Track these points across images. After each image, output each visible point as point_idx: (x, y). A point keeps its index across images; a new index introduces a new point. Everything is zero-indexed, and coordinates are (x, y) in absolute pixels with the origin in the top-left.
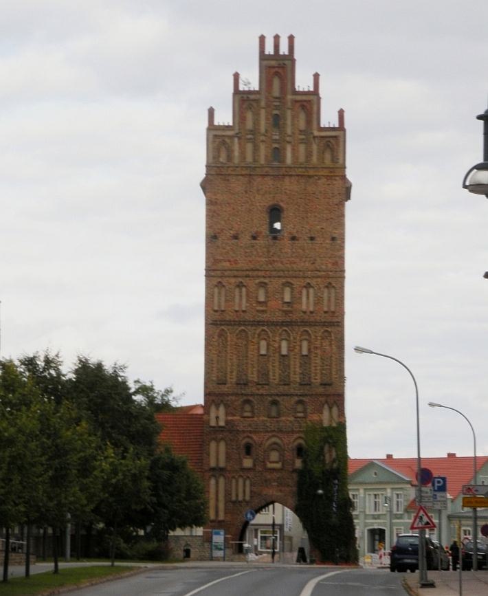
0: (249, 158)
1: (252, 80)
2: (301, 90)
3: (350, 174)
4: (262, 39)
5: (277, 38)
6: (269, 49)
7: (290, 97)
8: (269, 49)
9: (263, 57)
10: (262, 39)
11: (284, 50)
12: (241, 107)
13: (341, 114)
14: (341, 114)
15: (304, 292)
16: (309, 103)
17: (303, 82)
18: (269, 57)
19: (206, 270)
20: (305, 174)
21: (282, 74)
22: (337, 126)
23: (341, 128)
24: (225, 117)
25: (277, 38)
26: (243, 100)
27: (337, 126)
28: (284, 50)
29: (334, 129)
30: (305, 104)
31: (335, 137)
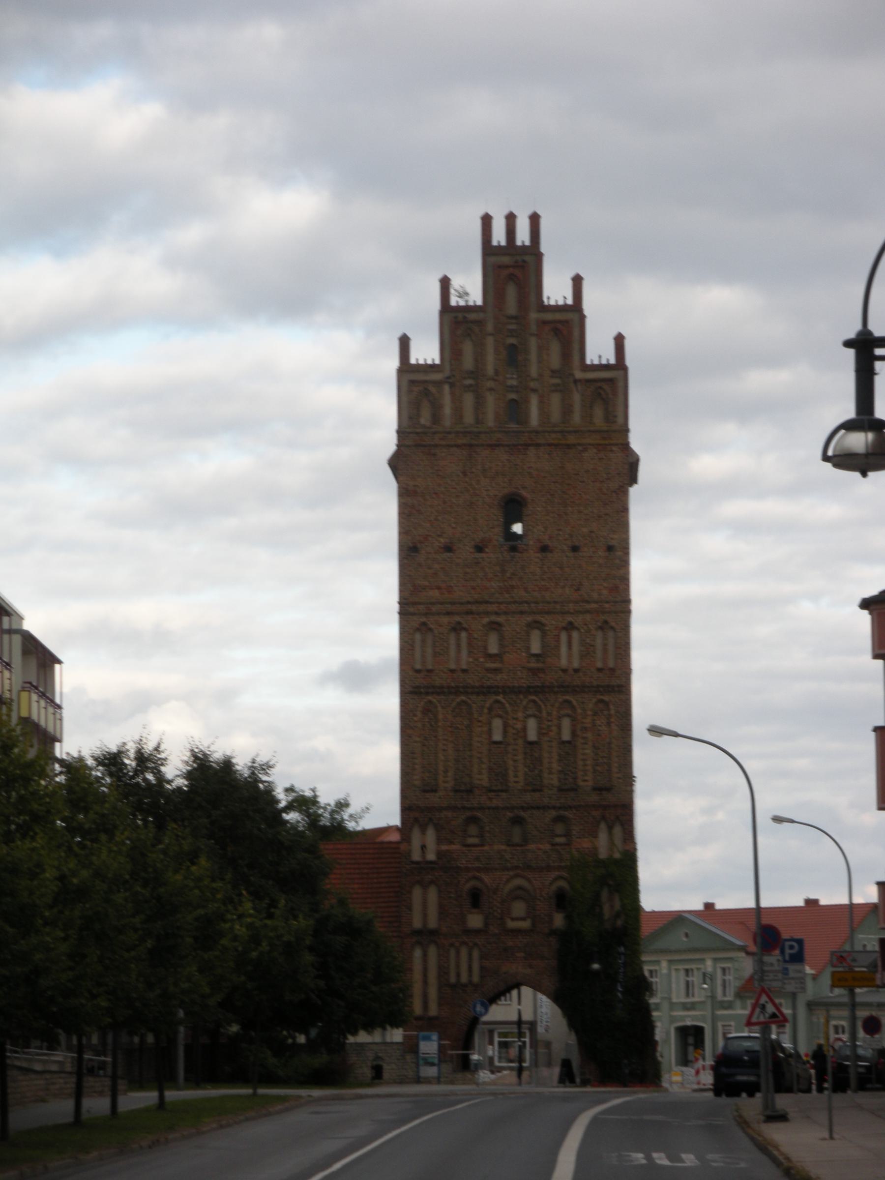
3: (636, 443)
4: (487, 221)
5: (511, 219)
6: (499, 237)
8: (499, 237)
10: (487, 221)
11: (523, 236)
13: (619, 341)
14: (619, 341)
22: (613, 361)
25: (511, 219)
27: (613, 361)
28: (523, 236)
29: (607, 367)
30: (559, 326)
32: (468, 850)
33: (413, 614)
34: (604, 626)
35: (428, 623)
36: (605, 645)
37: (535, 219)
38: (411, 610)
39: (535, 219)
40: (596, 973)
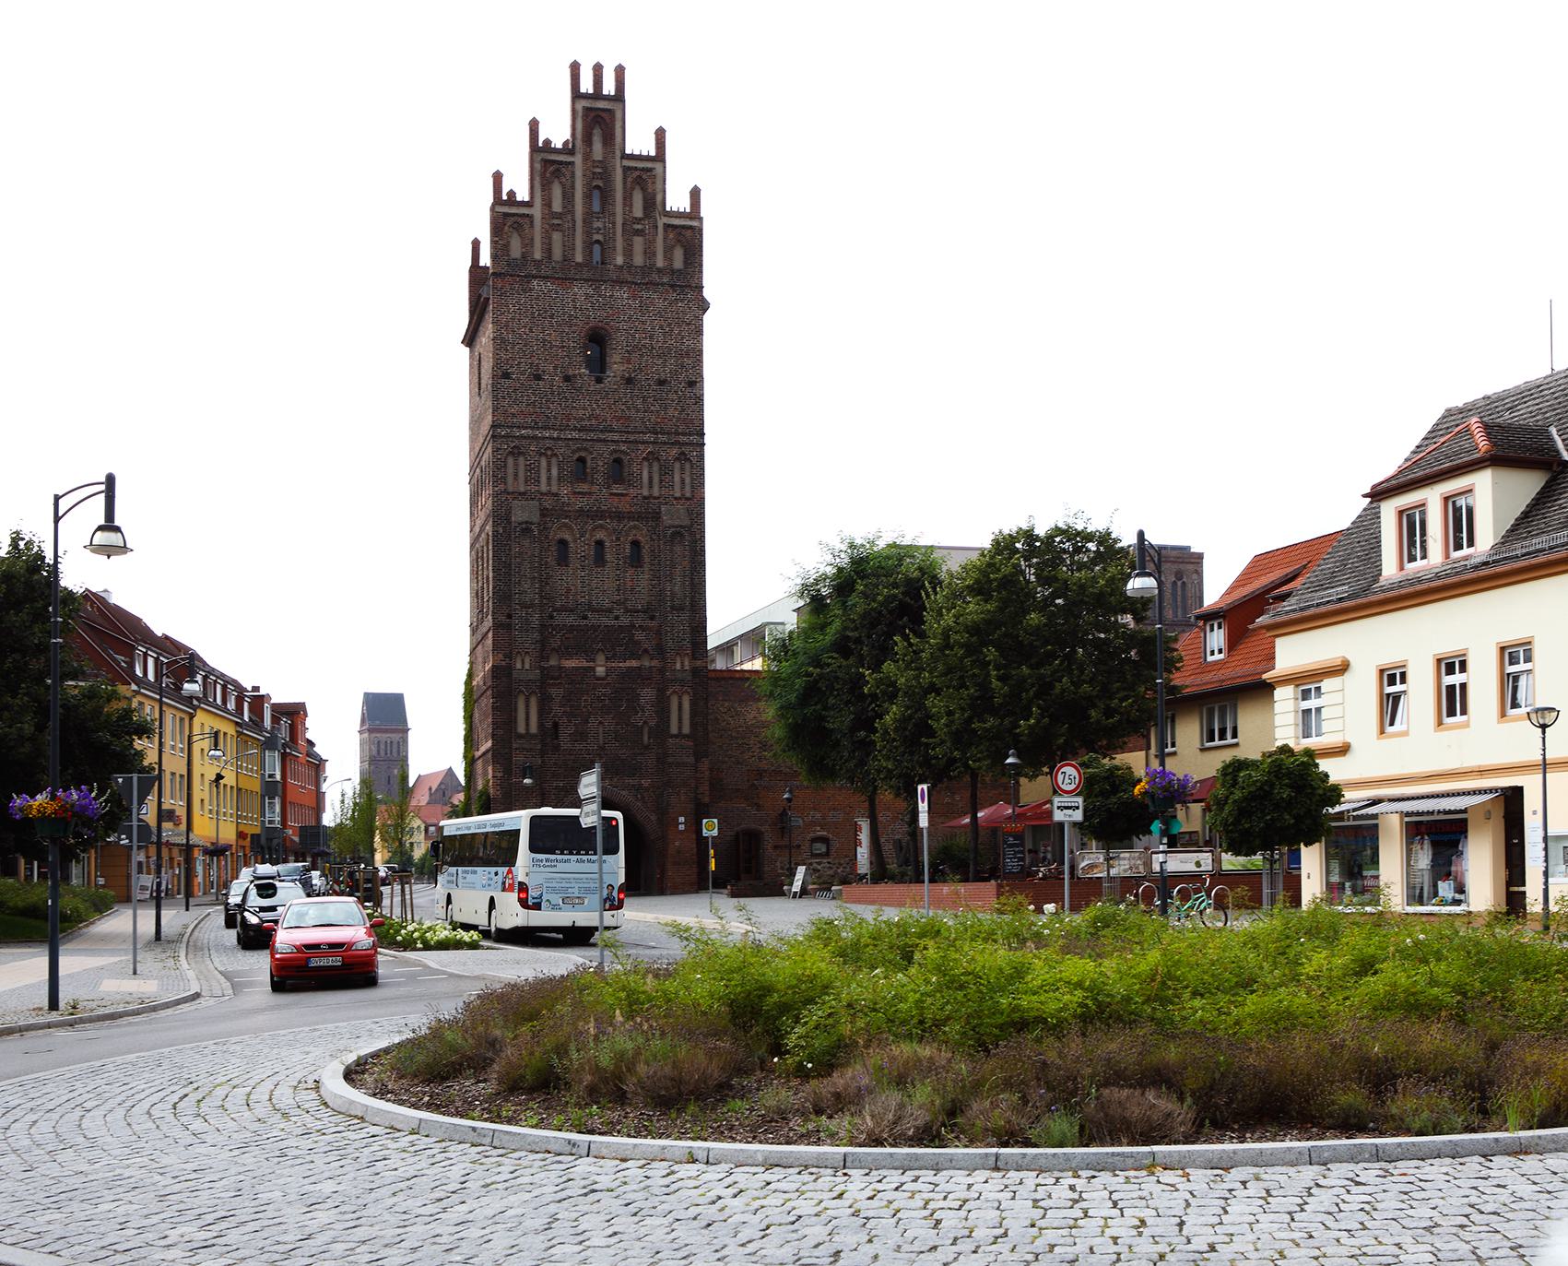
0: (557, 253)
1: (558, 131)
2: (675, 209)
3: (707, 293)
4: (575, 68)
5: (598, 70)
6: (587, 85)
7: (662, 221)
8: (587, 85)
9: (576, 94)
10: (575, 68)
11: (609, 87)
12: (543, 175)
13: (660, 135)
14: (660, 135)
15: (677, 465)
16: (648, 172)
17: (638, 141)
18: (586, 96)
19: (1004, 546)
20: (641, 279)
21: (608, 121)
22: (653, 153)
23: (660, 156)
24: (519, 184)
25: (598, 70)
26: (545, 161)
27: (653, 153)
28: (609, 87)
29: (648, 158)
30: (603, 115)
31: (650, 170)
32: (56, 1087)
33: (379, 746)
34: (682, 457)
35: (753, 826)
36: (683, 481)
37: (620, 71)
38: (382, 747)
39: (620, 71)
40: (526, 787)
